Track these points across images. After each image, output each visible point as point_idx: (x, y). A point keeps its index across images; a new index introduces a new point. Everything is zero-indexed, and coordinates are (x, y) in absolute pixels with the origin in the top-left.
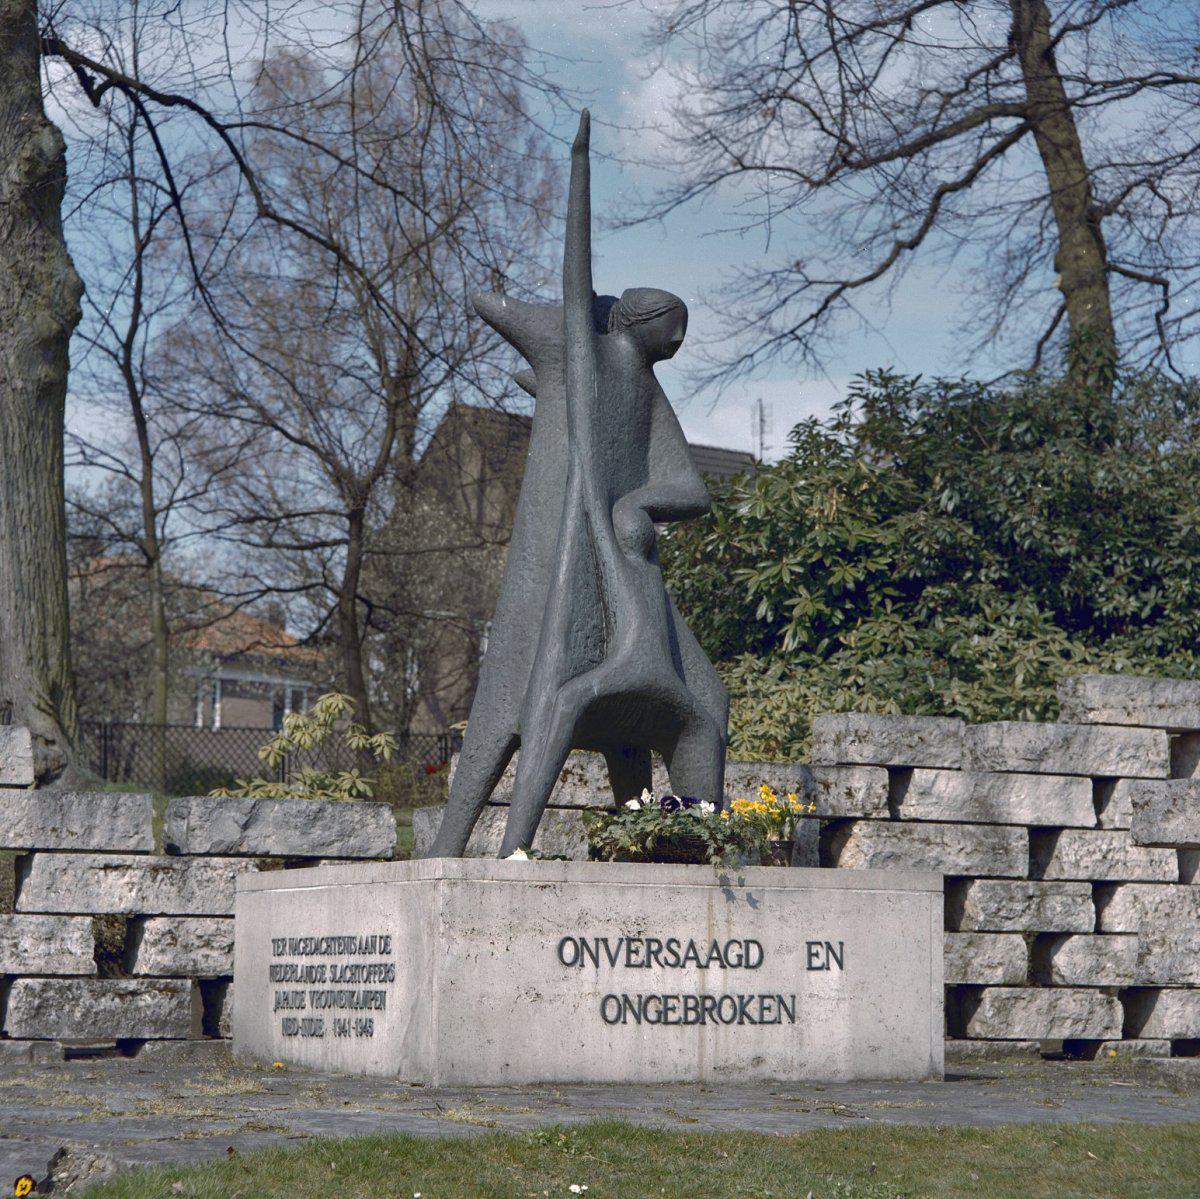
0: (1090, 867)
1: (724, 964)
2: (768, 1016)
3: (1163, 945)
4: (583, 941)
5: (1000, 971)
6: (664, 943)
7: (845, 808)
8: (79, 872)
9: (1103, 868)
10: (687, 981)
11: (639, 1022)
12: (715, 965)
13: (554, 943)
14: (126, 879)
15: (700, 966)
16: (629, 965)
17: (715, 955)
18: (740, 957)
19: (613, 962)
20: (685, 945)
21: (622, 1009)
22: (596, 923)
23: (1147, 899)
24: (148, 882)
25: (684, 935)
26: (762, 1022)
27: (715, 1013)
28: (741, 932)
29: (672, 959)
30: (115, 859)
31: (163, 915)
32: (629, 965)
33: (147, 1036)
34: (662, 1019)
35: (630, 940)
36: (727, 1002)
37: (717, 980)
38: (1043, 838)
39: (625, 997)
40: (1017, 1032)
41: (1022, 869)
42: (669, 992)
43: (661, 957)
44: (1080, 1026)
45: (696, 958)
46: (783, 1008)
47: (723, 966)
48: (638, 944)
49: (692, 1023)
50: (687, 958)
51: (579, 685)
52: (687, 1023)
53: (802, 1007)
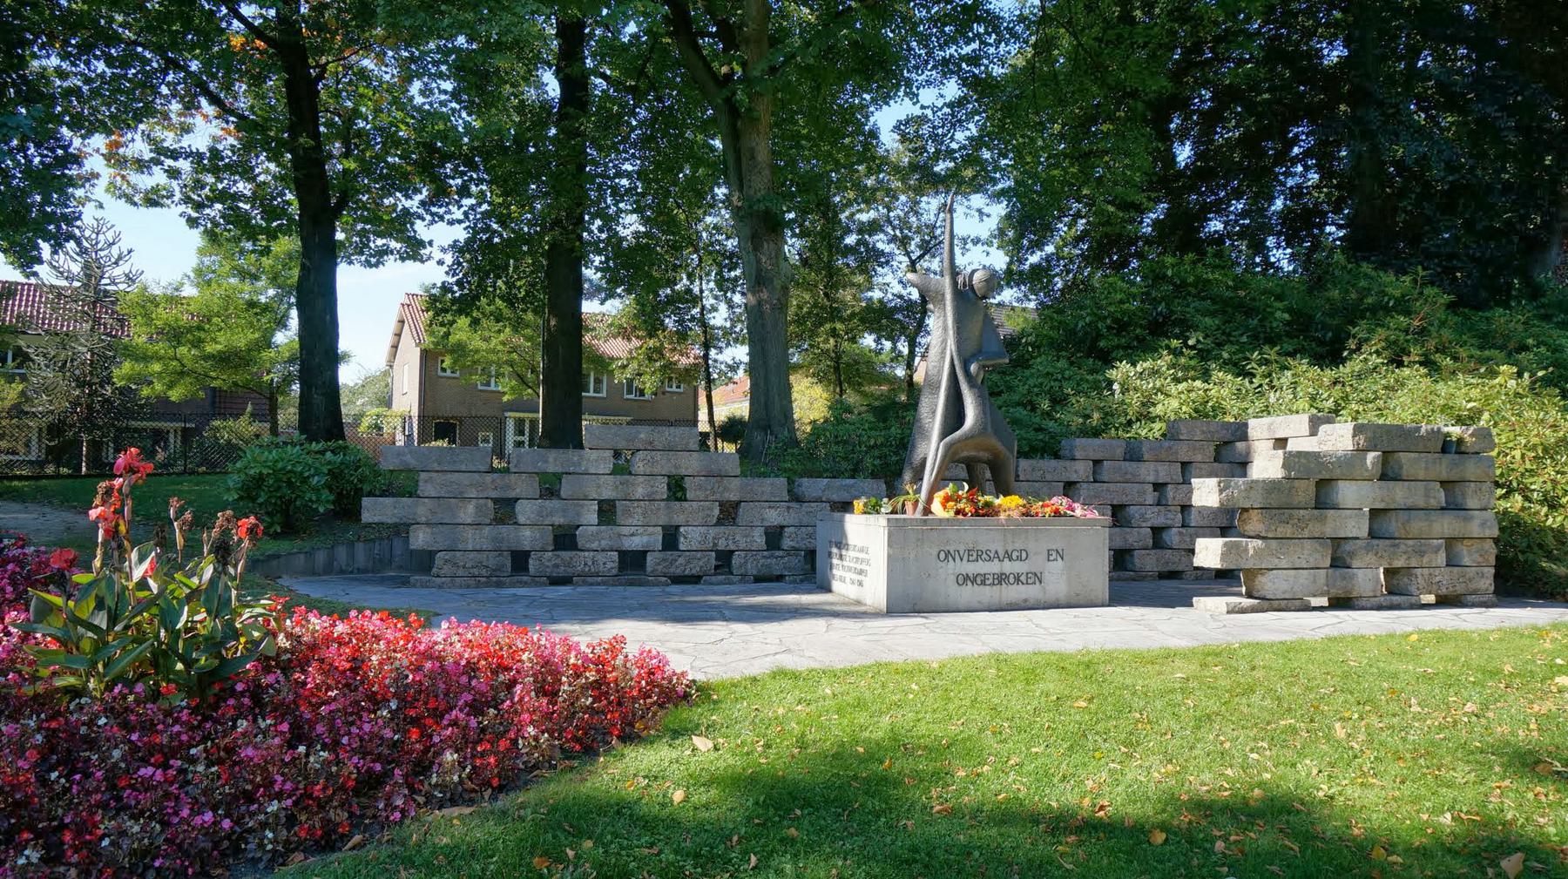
1: (1010, 559)
7: (1074, 478)
10: (994, 567)
13: (935, 553)
21: (967, 579)
25: (993, 548)
28: (1018, 546)
34: (983, 583)
37: (1008, 567)
40: (1148, 568)
46: (1038, 578)
51: (948, 439)
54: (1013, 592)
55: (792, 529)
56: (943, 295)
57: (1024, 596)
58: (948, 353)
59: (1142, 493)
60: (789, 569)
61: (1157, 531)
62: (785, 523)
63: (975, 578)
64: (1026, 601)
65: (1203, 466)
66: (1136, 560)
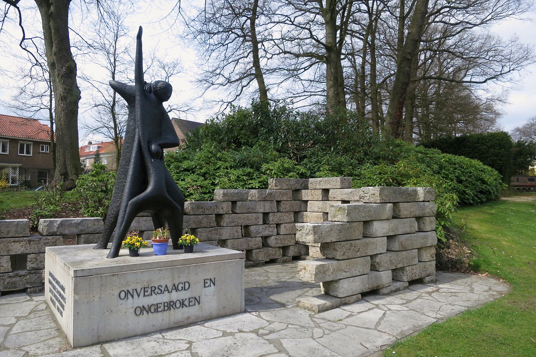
0: (276, 220)
1: (177, 290)
2: (191, 304)
3: (305, 270)
4: (128, 291)
5: (256, 246)
6: (157, 288)
7: (221, 212)
8: (5, 244)
9: (278, 221)
10: (165, 298)
11: (148, 313)
12: (174, 291)
13: (117, 293)
14: (21, 244)
15: (169, 292)
16: (144, 296)
17: (174, 288)
18: (182, 287)
19: (139, 296)
20: (164, 287)
22: (133, 284)
23: (287, 227)
24: (28, 245)
26: (189, 306)
27: (174, 306)
28: (183, 280)
29: (159, 292)
30: (17, 239)
31: (33, 253)
32: (144, 296)
33: (28, 287)
34: (156, 311)
35: (144, 288)
36: (178, 302)
37: (175, 296)
38: (266, 215)
39: (143, 307)
40: (260, 259)
41: (261, 222)
42: (158, 302)
43: (156, 291)
44: (273, 256)
45: (168, 290)
46: (197, 301)
47: (176, 291)
48: (148, 289)
49: (167, 310)
50: (165, 290)
51: (134, 199)
52: (164, 310)
53: (202, 300)
54: (179, 314)
55: (32, 256)
56: (134, 97)
57: (186, 315)
58: (137, 137)
59: (257, 219)
60: (31, 283)
61: (265, 238)
62: (27, 252)
63: (150, 308)
64: (188, 318)
65: (286, 202)
66: (254, 256)
